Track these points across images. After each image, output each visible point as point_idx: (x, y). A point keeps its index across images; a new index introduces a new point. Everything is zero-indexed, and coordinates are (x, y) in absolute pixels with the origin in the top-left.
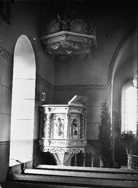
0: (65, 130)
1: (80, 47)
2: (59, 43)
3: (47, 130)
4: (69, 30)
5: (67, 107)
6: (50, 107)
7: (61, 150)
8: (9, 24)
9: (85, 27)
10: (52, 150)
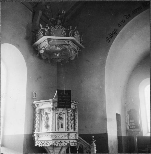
0: (50, 123)
1: (61, 48)
2: (45, 47)
3: (37, 125)
4: (50, 35)
5: (51, 102)
6: (38, 103)
7: (48, 143)
8: (88, 61)
9: (65, 31)
10: (40, 143)
